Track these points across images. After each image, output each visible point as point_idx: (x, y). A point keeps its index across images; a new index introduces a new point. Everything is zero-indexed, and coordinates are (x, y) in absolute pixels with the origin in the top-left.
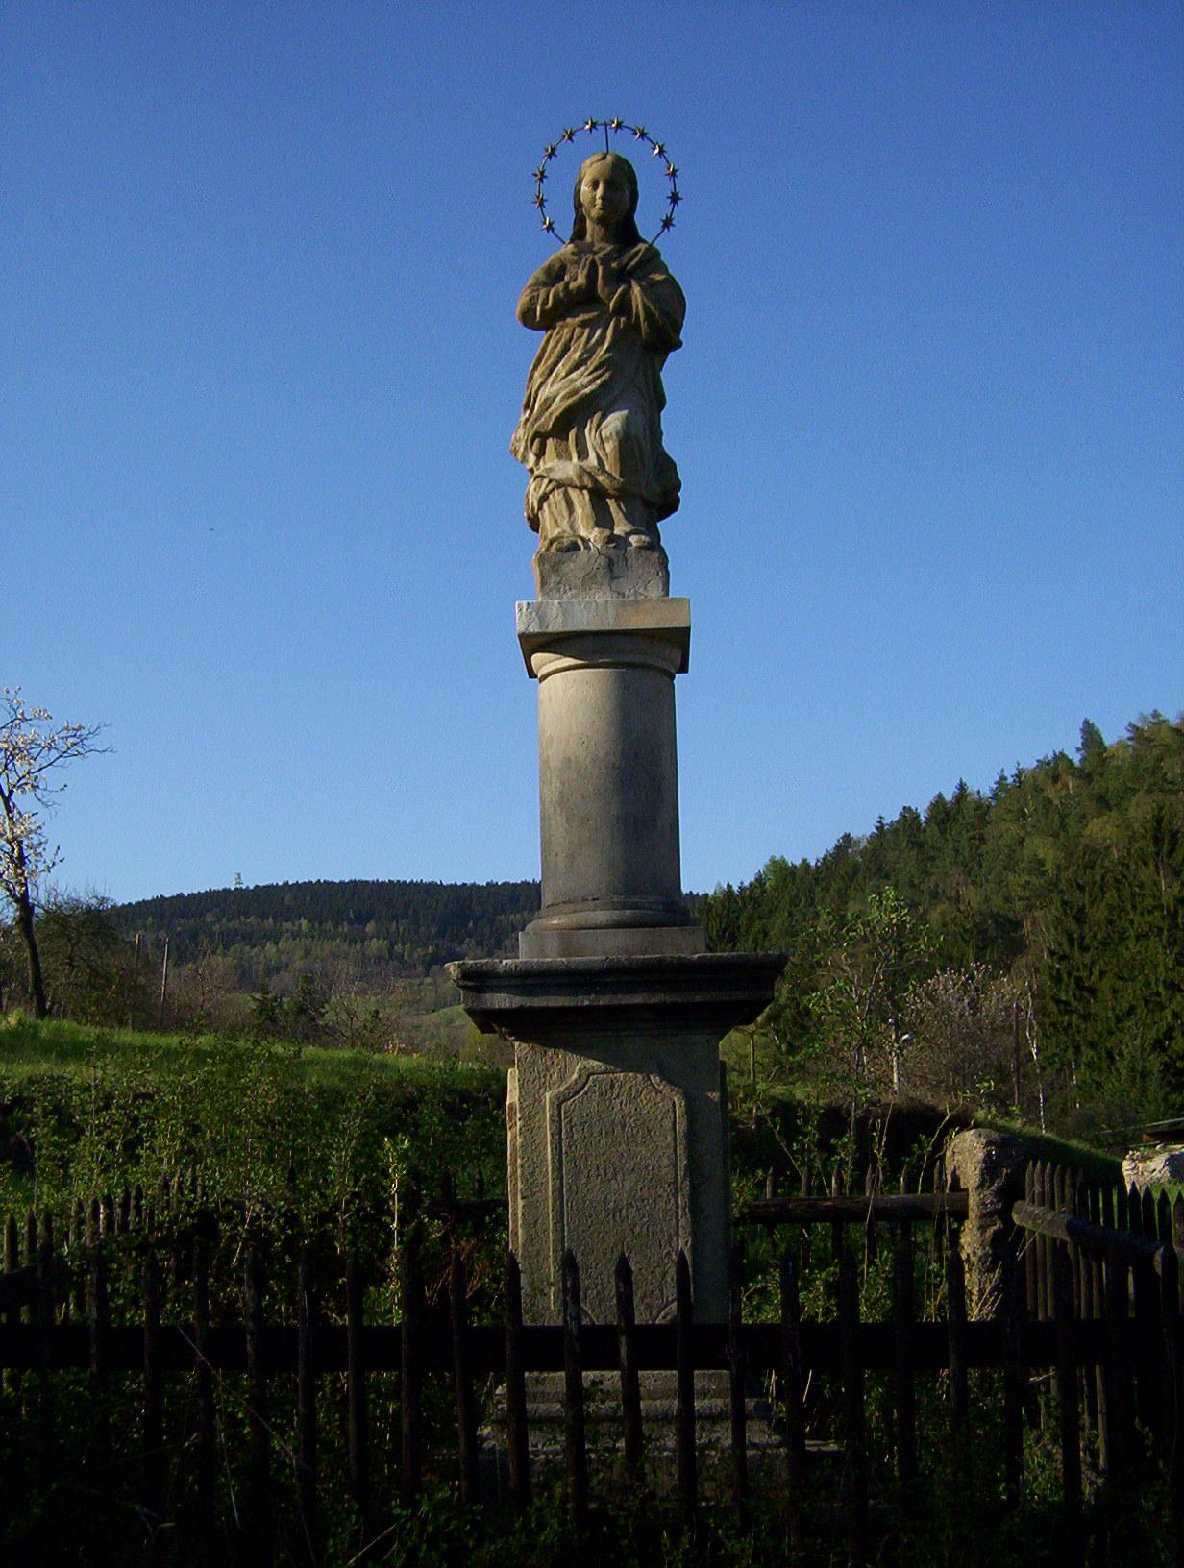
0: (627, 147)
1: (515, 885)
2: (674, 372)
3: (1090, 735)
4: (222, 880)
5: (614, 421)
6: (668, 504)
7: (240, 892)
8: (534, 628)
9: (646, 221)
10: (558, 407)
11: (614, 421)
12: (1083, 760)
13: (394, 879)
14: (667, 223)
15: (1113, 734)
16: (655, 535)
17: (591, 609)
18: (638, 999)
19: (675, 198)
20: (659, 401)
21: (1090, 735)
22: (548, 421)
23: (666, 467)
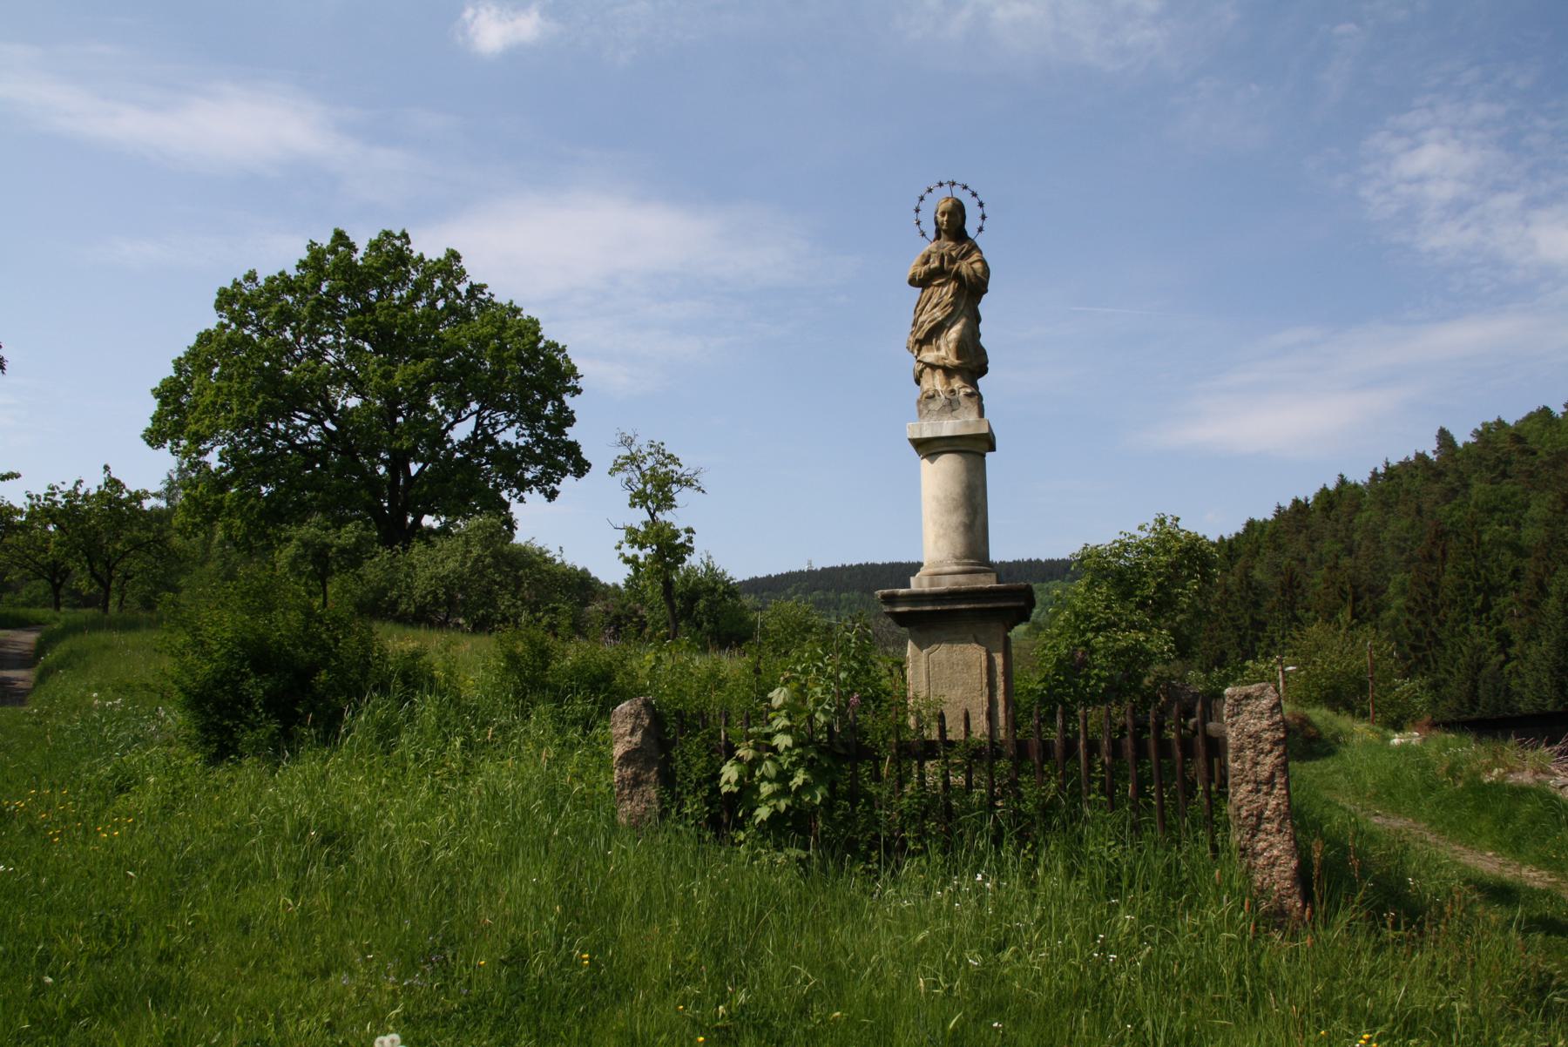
0: (959, 194)
1: (1009, 564)
2: (985, 306)
3: (1444, 437)
4: (798, 565)
5: (958, 327)
6: (983, 371)
7: (811, 573)
8: (916, 436)
9: (971, 228)
10: (927, 327)
11: (958, 327)
12: (690, 572)
13: (827, 566)
14: (981, 230)
15: (1463, 437)
16: (977, 387)
17: (948, 427)
18: (929, 608)
19: (983, 217)
20: (978, 319)
21: (1444, 437)
22: (921, 335)
23: (981, 355)
